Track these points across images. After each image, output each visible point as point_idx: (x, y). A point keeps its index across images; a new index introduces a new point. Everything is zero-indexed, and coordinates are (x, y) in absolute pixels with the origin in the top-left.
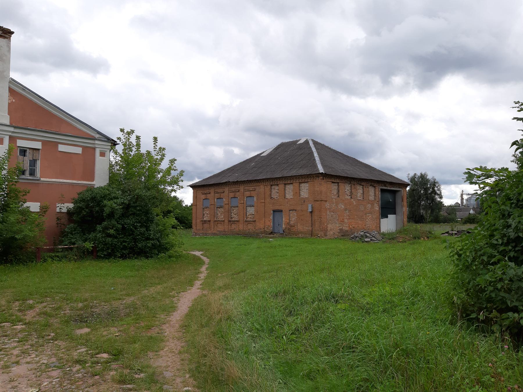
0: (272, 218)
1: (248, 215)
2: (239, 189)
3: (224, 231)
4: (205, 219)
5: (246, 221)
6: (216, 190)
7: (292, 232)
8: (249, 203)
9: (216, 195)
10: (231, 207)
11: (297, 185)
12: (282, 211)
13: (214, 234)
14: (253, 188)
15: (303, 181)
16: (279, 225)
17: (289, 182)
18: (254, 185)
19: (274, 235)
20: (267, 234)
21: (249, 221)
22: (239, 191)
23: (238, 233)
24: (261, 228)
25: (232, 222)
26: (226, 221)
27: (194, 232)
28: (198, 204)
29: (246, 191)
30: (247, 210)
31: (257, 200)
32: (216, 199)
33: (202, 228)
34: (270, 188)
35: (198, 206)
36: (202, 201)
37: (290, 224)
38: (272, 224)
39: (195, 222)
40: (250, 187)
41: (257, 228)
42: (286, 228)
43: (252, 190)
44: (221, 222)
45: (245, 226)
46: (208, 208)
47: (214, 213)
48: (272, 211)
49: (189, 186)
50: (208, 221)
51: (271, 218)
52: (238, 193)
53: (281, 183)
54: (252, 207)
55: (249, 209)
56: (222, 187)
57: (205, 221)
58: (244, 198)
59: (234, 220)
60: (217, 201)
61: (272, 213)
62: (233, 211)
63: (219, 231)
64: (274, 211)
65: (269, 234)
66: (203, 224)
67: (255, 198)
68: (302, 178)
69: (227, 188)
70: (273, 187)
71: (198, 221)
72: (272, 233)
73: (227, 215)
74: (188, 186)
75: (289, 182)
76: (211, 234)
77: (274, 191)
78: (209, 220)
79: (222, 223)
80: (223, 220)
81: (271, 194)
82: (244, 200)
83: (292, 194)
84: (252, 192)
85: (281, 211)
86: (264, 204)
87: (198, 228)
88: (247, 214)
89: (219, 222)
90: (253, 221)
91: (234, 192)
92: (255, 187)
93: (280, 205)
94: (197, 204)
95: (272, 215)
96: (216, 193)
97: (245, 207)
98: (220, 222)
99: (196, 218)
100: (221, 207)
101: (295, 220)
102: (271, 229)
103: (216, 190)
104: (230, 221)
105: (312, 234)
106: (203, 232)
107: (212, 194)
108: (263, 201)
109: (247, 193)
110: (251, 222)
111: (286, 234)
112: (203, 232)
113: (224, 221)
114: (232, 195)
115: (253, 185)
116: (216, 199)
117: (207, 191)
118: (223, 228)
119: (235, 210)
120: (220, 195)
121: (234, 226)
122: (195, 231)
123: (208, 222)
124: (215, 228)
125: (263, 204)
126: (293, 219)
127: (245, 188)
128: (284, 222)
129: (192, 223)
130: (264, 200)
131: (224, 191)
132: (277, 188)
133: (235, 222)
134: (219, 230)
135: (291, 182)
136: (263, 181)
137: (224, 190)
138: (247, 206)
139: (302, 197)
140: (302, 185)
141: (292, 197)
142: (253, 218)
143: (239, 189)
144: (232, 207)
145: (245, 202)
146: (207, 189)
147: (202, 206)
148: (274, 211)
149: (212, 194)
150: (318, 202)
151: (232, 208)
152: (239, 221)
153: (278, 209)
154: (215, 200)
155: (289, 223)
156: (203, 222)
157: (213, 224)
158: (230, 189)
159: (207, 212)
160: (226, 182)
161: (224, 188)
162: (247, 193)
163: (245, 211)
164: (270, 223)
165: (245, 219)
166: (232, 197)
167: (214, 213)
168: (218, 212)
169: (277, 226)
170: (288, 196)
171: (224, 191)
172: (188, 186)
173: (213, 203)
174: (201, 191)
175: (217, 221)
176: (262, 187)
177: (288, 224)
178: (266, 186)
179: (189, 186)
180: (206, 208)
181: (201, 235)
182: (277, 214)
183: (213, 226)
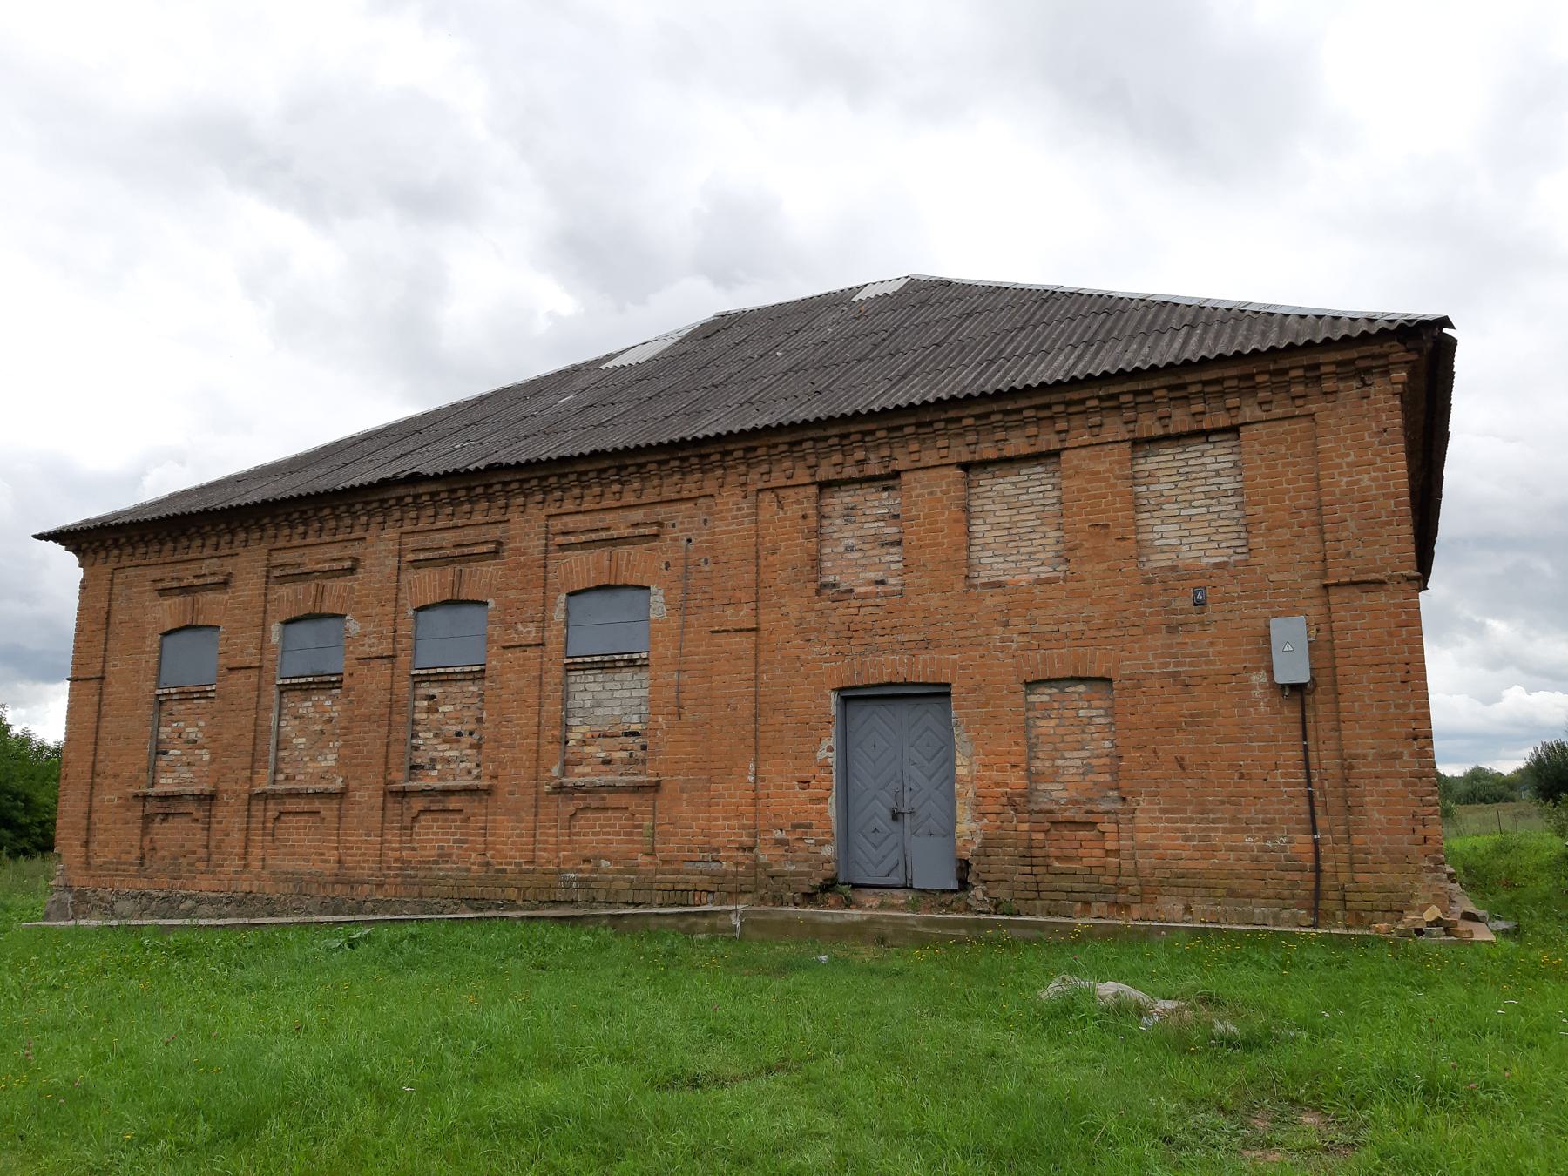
0: (832, 758)
1: (575, 736)
2: (496, 532)
3: (338, 880)
4: (167, 783)
5: (561, 789)
6: (279, 558)
7: (1065, 884)
8: (587, 643)
9: (284, 591)
10: (418, 680)
11: (801, 502)
12: (948, 694)
13: (240, 903)
14: (638, 515)
15: (1180, 421)
16: (896, 816)
17: (1017, 444)
18: (649, 496)
19: (848, 903)
20: (778, 900)
21: (591, 790)
22: (495, 553)
23: (477, 891)
24: (715, 842)
25: (418, 804)
26: (367, 796)
27: (69, 888)
28: (115, 667)
29: (564, 547)
30: (565, 698)
31: (682, 608)
32: (275, 629)
33: (136, 853)
34: (809, 507)
35: (114, 688)
36: (152, 642)
37: (1042, 803)
38: (831, 810)
39: (83, 807)
40: (610, 518)
41: (671, 847)
42: (990, 844)
43: (626, 532)
44: (317, 805)
45: (392, 837)
46: (204, 695)
47: (258, 731)
48: (834, 698)
49: (58, 536)
50: (199, 798)
51: (827, 753)
52: (489, 571)
53: (930, 457)
54: (627, 675)
55: (587, 688)
56: (304, 535)
57: (165, 798)
58: (546, 604)
59: (438, 785)
60: (283, 637)
61: (833, 710)
62: (431, 710)
63: (289, 878)
64: (851, 697)
65: (809, 897)
66: (147, 820)
67: (657, 598)
68: (1179, 393)
69: (391, 533)
70: (838, 501)
71: (109, 796)
72: (829, 886)
73: (379, 747)
74: (41, 537)
75: (1017, 444)
76: (211, 902)
77: (841, 534)
78: (206, 788)
79: (328, 809)
80: (338, 784)
81: (816, 561)
82: (543, 623)
83: (1045, 541)
84: (624, 550)
85: (940, 693)
86: (747, 640)
87: (104, 853)
88: (567, 728)
89: (290, 805)
90: (638, 788)
91: (449, 560)
92: (662, 512)
93: (926, 644)
94: (110, 667)
95: (833, 731)
96: (282, 579)
97: (554, 677)
98: (303, 805)
99: (94, 773)
100: (322, 684)
101: (1088, 769)
102: (828, 851)
103: (279, 558)
104: (404, 793)
105: (1317, 894)
106: (142, 883)
107: (249, 586)
108: (744, 616)
109: (584, 566)
110: (612, 800)
111: (1001, 893)
112: (142, 883)
113: (342, 794)
114: (429, 584)
115: (217, 547)
116: (275, 629)
117: (207, 567)
118: (332, 856)
119: (454, 706)
120: (321, 591)
121: (433, 836)
122: (79, 880)
123: (191, 807)
124: (256, 852)
125: (738, 638)
126: (1073, 760)
127: (557, 525)
128: (966, 793)
129: (53, 823)
130: (745, 610)
131: (355, 560)
132: (876, 502)
133: (453, 803)
134: (288, 866)
135: (1049, 441)
136: (129, 538)
137: (357, 550)
138: (569, 668)
139: (1161, 561)
140: (991, 486)
141: (1045, 572)
142: (632, 760)
143: (496, 532)
144: (427, 678)
145: (553, 635)
146: (207, 552)
147: (150, 685)
148: (851, 697)
149: (249, 586)
150: (1382, 598)
151: (425, 689)
152: (489, 791)
153: (903, 674)
154: (264, 627)
155: (1028, 795)
156: (151, 808)
157: (237, 822)
158: (411, 542)
159: (189, 724)
160: (384, 484)
161: (357, 534)
162: (584, 566)
163: (551, 708)
164: (815, 800)
165: (556, 770)
166: (431, 598)
167: (258, 731)
168: (289, 726)
169: (882, 821)
170: (992, 565)
171: (499, 543)
172: (41, 537)
173: (250, 656)
174: (155, 573)
175: (274, 795)
176: (729, 500)
177: (1018, 802)
178: (767, 498)
179: (58, 536)
180: (186, 696)
181: (124, 906)
182: (876, 722)
183: (237, 837)
